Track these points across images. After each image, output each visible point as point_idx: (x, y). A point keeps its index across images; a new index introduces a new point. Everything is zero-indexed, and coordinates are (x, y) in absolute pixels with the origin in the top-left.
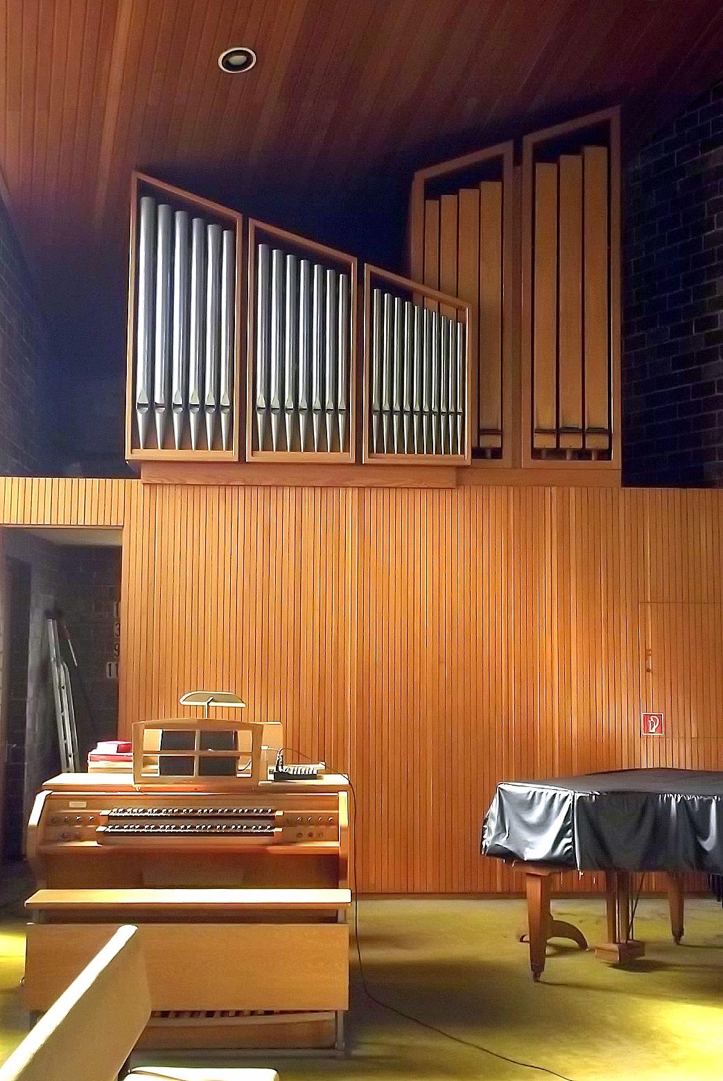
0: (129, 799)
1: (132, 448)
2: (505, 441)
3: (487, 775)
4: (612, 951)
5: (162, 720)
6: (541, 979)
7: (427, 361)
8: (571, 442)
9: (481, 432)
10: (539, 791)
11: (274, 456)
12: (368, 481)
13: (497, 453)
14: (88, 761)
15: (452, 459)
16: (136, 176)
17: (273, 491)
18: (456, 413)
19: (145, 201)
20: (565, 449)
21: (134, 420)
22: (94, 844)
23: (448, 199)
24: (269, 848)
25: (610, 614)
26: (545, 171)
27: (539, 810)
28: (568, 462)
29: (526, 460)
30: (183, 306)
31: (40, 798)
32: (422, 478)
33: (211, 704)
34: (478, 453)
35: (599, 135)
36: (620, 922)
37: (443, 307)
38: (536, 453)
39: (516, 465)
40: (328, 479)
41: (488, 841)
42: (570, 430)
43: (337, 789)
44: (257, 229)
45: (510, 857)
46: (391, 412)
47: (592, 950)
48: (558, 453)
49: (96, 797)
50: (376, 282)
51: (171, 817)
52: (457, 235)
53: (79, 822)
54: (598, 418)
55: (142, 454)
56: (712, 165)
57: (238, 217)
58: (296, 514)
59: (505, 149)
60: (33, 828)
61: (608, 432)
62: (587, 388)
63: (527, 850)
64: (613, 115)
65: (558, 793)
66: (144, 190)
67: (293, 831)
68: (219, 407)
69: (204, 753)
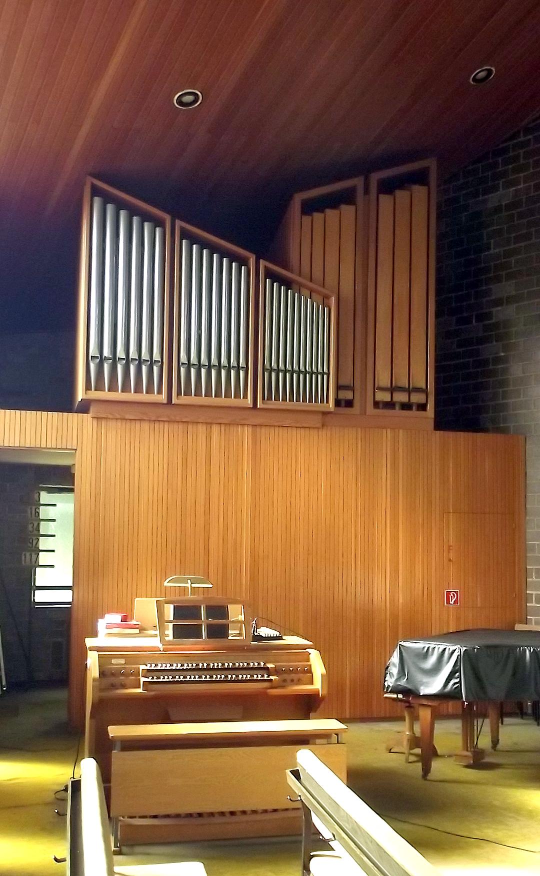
0: (157, 657)
5: (173, 598)
6: (428, 778)
7: (303, 332)
8: (401, 397)
9: (339, 388)
11: (192, 400)
13: (349, 404)
16: (90, 180)
18: (323, 374)
19: (97, 201)
23: (318, 216)
26: (385, 199)
27: (432, 660)
28: (397, 412)
30: (123, 286)
32: (296, 419)
34: (338, 403)
35: (420, 178)
36: (469, 734)
37: (314, 295)
38: (376, 404)
40: (229, 418)
41: (390, 681)
42: (401, 389)
43: (304, 647)
45: (410, 693)
46: (219, 367)
47: (443, 756)
48: (390, 405)
50: (269, 274)
52: (322, 240)
53: (122, 674)
55: (94, 395)
56: (490, 205)
57: (168, 218)
59: (358, 182)
62: (410, 359)
64: (431, 163)
66: (95, 192)
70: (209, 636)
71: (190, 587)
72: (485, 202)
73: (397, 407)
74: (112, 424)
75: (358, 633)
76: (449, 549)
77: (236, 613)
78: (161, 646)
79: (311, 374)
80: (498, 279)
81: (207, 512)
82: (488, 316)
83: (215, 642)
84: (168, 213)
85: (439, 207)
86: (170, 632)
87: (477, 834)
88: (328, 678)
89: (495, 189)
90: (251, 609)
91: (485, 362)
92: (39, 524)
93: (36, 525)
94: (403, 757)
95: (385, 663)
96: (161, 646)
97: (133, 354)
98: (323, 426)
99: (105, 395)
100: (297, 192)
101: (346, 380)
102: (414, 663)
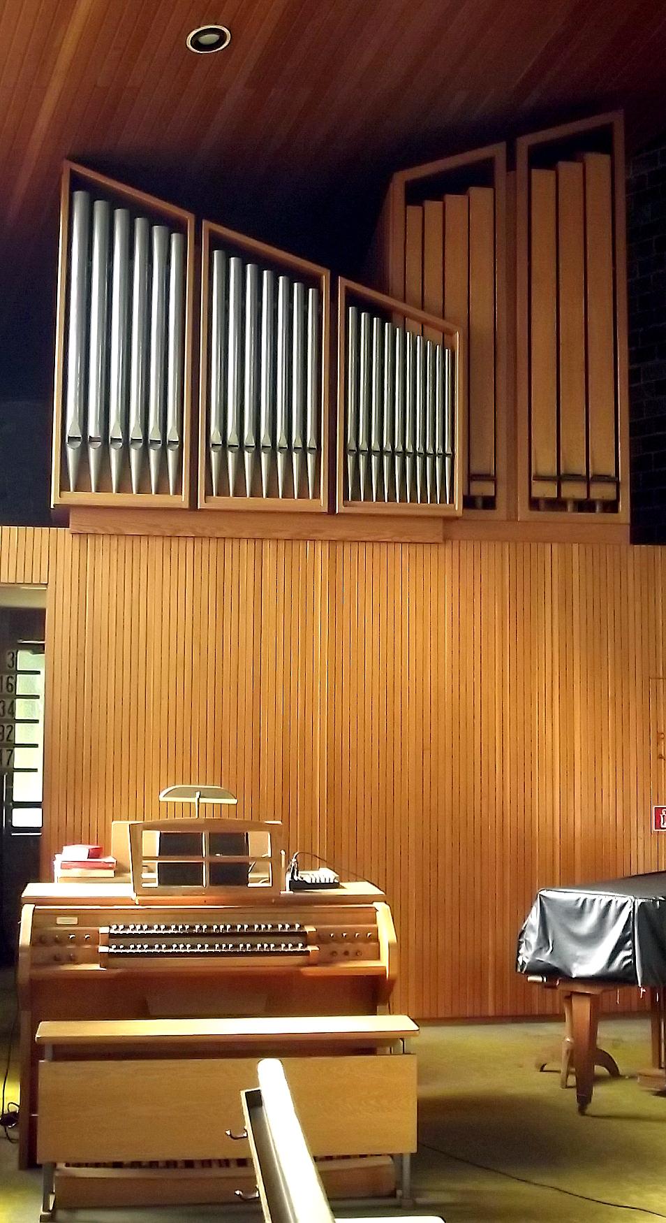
1: (61, 490)
2: (499, 490)
3: (478, 879)
4: (658, 1077)
8: (574, 491)
9: (471, 477)
10: (590, 898)
11: (230, 502)
13: (489, 503)
15: (409, 508)
16: (68, 166)
17: (228, 544)
18: (444, 455)
19: (79, 196)
21: (61, 457)
22: (96, 967)
23: (432, 207)
25: (619, 693)
26: (542, 178)
28: (570, 514)
29: (523, 511)
30: (123, 320)
34: (469, 502)
35: (600, 141)
38: (534, 503)
39: (512, 517)
40: (297, 530)
41: (526, 956)
42: (574, 478)
43: (370, 899)
45: (555, 974)
48: (557, 504)
49: (89, 912)
50: (353, 299)
51: (185, 935)
52: (443, 245)
53: (72, 941)
55: (73, 497)
58: (259, 571)
59: (497, 151)
60: (24, 948)
61: (615, 481)
62: (592, 434)
63: (575, 965)
64: (616, 119)
65: (598, 898)
66: (77, 183)
70: (214, 881)
71: (189, 801)
73: (570, 507)
75: (508, 877)
77: (260, 844)
78: (133, 896)
79: (434, 456)
81: (257, 680)
83: (221, 892)
84: (189, 210)
85: (629, 187)
86: (151, 877)
87: (634, 1200)
88: (399, 948)
90: (280, 839)
92: (13, 704)
93: (8, 704)
94: (557, 1078)
95: (518, 927)
96: (137, 900)
97: (135, 432)
98: (445, 540)
99: (91, 497)
100: (397, 170)
101: (483, 464)
102: (563, 925)
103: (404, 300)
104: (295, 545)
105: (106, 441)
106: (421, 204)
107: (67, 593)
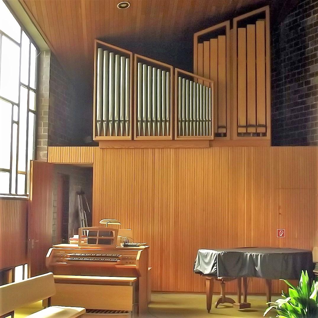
7: (198, 101)
8: (252, 130)
12: (178, 146)
14: (70, 240)
16: (96, 41)
20: (250, 132)
21: (96, 126)
23: (206, 43)
24: (116, 266)
26: (242, 30)
27: (209, 258)
31: (51, 250)
33: (108, 223)
34: (217, 135)
35: (262, 16)
38: (239, 134)
40: (163, 145)
42: (251, 126)
44: (137, 58)
45: (200, 273)
48: (247, 134)
50: (180, 74)
52: (208, 54)
54: (262, 121)
55: (98, 138)
56: (309, 23)
57: (171, 67)
59: (227, 23)
60: (47, 257)
61: (266, 126)
64: (266, 9)
66: (99, 46)
67: (124, 261)
68: (125, 121)
69: (100, 238)
72: (306, 22)
74: (109, 151)
76: (279, 209)
80: (312, 63)
82: (308, 83)
89: (309, 15)
91: (307, 108)
101: (223, 123)
102: (203, 259)
103: (198, 75)
104: (165, 150)
105: (114, 121)
106: (245, 27)
107: (99, 165)
